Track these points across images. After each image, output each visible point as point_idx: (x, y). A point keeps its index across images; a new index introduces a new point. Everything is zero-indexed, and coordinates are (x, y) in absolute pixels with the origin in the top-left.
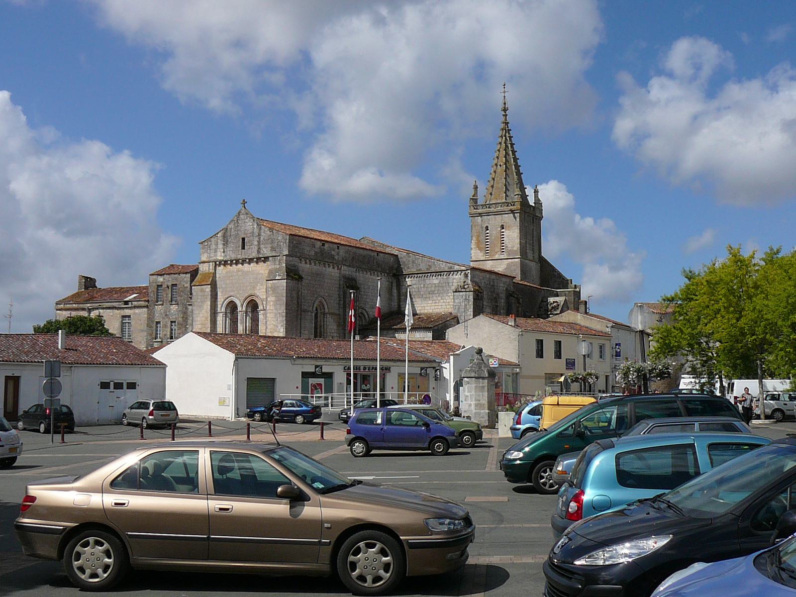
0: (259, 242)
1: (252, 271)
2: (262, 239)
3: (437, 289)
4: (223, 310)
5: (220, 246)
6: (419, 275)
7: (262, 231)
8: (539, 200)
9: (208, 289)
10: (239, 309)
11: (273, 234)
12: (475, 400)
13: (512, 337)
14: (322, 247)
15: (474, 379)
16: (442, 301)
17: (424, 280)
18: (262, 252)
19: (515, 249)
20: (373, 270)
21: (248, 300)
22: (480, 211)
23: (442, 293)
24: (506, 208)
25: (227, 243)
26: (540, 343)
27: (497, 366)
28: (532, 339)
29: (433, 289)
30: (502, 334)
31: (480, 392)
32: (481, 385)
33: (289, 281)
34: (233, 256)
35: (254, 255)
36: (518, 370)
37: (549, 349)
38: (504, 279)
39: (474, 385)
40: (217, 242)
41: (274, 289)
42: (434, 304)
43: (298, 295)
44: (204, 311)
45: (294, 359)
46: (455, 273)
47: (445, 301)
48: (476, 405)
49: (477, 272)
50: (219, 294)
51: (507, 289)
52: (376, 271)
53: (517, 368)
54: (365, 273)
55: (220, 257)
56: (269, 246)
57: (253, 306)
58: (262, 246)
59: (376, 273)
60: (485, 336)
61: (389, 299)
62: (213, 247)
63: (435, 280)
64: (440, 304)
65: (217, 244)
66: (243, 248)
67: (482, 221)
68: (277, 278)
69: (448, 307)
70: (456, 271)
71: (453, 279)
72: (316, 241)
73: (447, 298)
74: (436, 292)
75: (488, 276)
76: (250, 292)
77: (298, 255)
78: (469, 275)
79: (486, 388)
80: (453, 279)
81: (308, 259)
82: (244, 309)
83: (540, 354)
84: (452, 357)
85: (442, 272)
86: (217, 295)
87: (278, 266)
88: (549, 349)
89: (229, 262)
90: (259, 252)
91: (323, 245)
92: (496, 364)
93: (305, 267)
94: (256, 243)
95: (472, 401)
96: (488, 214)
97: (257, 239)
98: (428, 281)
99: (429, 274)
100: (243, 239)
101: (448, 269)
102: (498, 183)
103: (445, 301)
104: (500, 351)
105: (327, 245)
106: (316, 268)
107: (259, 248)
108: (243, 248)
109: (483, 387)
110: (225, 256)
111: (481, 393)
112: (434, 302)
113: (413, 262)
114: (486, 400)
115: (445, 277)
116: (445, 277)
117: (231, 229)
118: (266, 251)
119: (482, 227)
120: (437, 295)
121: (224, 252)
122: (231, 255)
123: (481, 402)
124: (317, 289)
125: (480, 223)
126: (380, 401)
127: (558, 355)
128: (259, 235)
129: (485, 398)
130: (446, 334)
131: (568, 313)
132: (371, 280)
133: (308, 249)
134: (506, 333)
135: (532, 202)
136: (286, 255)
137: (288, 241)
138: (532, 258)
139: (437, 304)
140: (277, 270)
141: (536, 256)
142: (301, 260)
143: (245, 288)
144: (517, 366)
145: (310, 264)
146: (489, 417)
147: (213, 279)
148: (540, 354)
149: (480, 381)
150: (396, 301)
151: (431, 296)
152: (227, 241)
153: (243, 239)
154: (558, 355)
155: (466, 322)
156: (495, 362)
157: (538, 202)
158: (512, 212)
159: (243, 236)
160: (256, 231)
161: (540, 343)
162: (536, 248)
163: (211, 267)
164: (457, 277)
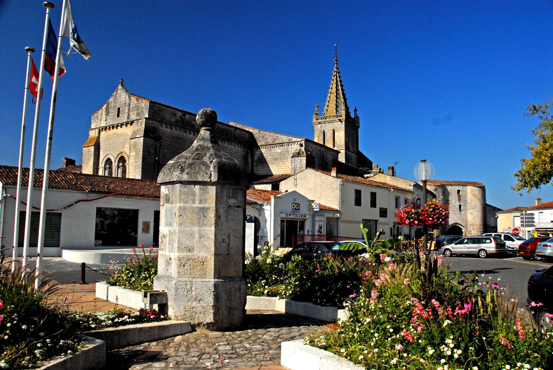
0: (129, 110)
1: (124, 133)
2: (131, 107)
3: (280, 156)
4: (103, 165)
5: (104, 116)
6: (267, 146)
7: (132, 101)
8: (357, 116)
9: (92, 149)
10: (114, 164)
11: (138, 103)
12: (180, 249)
13: (334, 187)
14: (183, 117)
15: (178, 186)
16: (283, 165)
17: (270, 150)
18: (130, 118)
19: (342, 144)
20: (231, 141)
21: (119, 156)
22: (320, 121)
23: (283, 160)
24: (337, 119)
25: (108, 114)
26: (358, 193)
27: (318, 210)
28: (352, 188)
29: (277, 156)
30: (326, 184)
31: (193, 224)
32: (197, 205)
33: (147, 139)
34: (112, 123)
35: (125, 120)
36: (338, 215)
37: (366, 199)
38: (331, 153)
39: (179, 205)
40: (102, 113)
41: (135, 145)
42: (277, 168)
43: (156, 151)
44: (89, 167)
45: (86, 193)
46: (293, 144)
47: (285, 165)
48: (182, 264)
49: (310, 144)
50: (101, 153)
51: (333, 159)
52: (233, 142)
53: (337, 213)
54: (224, 142)
55: (103, 124)
56: (136, 112)
57: (122, 160)
58: (131, 113)
59: (233, 144)
60: (311, 186)
61: (245, 164)
62: (100, 117)
63: (278, 150)
64: (282, 167)
65: (102, 115)
66: (118, 116)
67: (321, 127)
68: (137, 136)
69: (288, 169)
70: (294, 142)
71: (292, 148)
72: (177, 111)
73: (287, 163)
74: (278, 159)
75: (319, 148)
76: (121, 150)
77: (159, 119)
78: (304, 144)
79: (212, 215)
80: (292, 148)
81: (168, 124)
82: (116, 164)
83: (358, 202)
84: (273, 200)
85: (283, 143)
86: (99, 154)
87: (140, 127)
88: (366, 199)
89: (108, 127)
90: (128, 118)
91: (184, 115)
92: (317, 208)
93: (165, 130)
94: (127, 111)
95: (171, 250)
96: (325, 123)
97: (127, 108)
98: (273, 151)
99: (274, 145)
100: (119, 109)
101: (289, 140)
102: (331, 104)
103: (285, 165)
104: (324, 199)
105: (187, 116)
106: (176, 132)
107: (129, 115)
108: (118, 116)
109: (203, 211)
110: (107, 123)
111: (196, 229)
112: (277, 166)
113: (263, 137)
114: (208, 249)
115: (286, 147)
116: (286, 147)
117: (111, 102)
118: (133, 117)
119: (321, 131)
120: (280, 161)
121: (106, 120)
122: (110, 122)
123: (196, 252)
124: (177, 150)
125: (320, 129)
126: (326, 241)
127: (373, 204)
128: (129, 104)
129: (206, 243)
130: (280, 185)
131: (380, 176)
132: (228, 148)
133: (169, 116)
134: (329, 183)
135: (352, 115)
136: (146, 118)
137: (148, 107)
138: (352, 151)
139: (279, 168)
140: (138, 131)
141: (356, 151)
142: (161, 124)
143: (118, 148)
144: (337, 211)
145: (171, 129)
146: (217, 298)
147: (96, 141)
148: (358, 202)
149: (193, 194)
150: (250, 166)
151: (275, 161)
152: (109, 112)
153: (119, 109)
154: (373, 204)
155: (295, 176)
156: (316, 206)
157: (357, 117)
158: (340, 120)
159: (119, 107)
160: (128, 101)
161: (358, 193)
162: (355, 145)
163: (96, 133)
164: (294, 146)
